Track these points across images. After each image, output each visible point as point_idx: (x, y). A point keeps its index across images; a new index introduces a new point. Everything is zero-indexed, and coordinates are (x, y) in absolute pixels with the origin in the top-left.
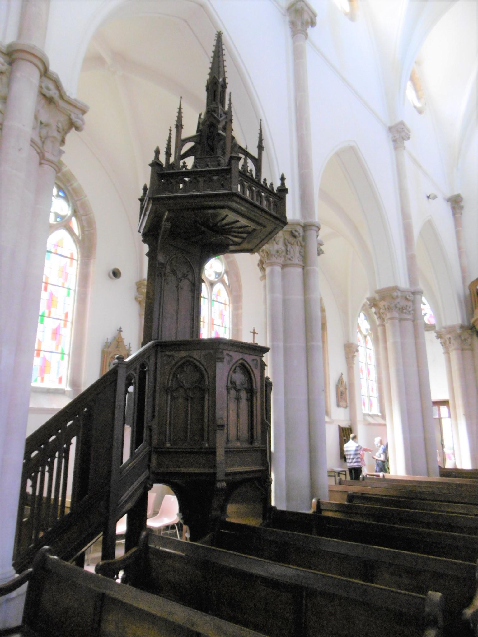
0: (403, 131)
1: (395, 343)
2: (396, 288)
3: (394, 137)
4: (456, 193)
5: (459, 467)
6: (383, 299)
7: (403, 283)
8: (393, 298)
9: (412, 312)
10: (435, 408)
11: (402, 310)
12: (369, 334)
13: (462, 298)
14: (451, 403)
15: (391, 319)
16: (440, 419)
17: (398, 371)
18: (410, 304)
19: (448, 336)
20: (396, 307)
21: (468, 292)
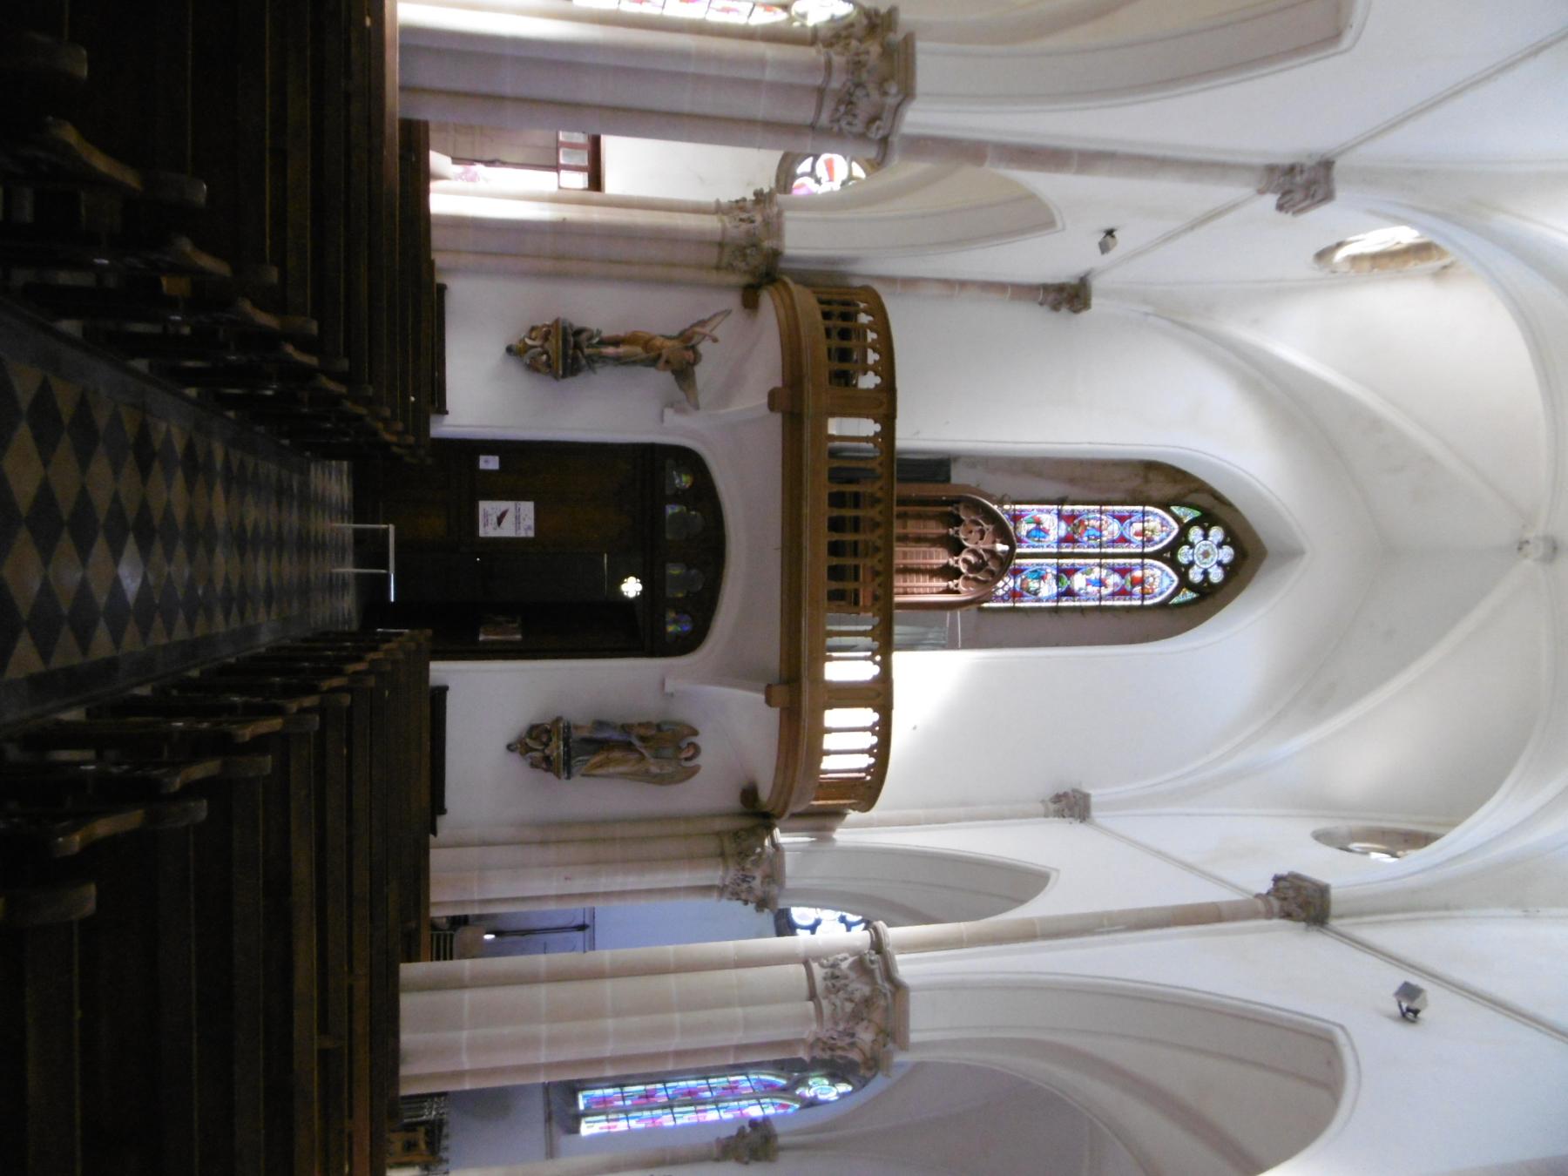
0: (1306, 197)
1: (762, 63)
2: (908, 94)
3: (1302, 172)
4: (1095, 301)
5: (434, 185)
6: (888, 52)
7: (918, 118)
8: (882, 83)
9: (836, 129)
10: (580, 138)
11: (847, 101)
12: (791, 19)
13: (842, 268)
14: (595, 195)
15: (829, 66)
16: (556, 168)
17: (685, 55)
18: (859, 126)
19: (758, 218)
20: (859, 85)
21: (857, 283)
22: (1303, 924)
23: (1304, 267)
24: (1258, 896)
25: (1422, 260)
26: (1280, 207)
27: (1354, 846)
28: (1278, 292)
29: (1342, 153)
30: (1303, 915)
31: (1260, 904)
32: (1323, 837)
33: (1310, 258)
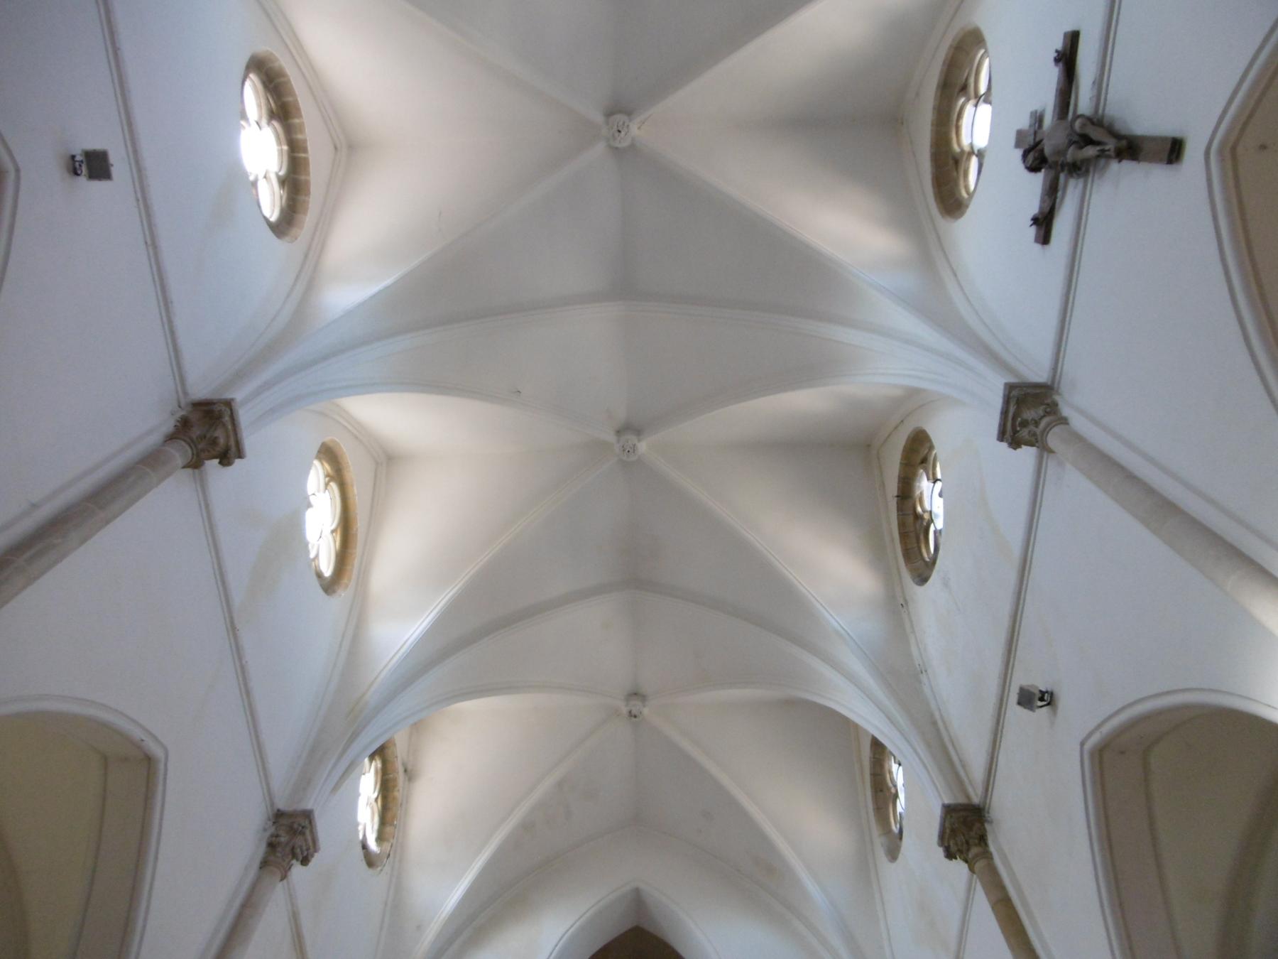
0: (302, 833)
22: (987, 826)
23: (378, 880)
24: (972, 870)
25: (395, 786)
26: (305, 861)
28: (396, 905)
29: (272, 804)
30: (977, 825)
31: (979, 865)
33: (371, 871)
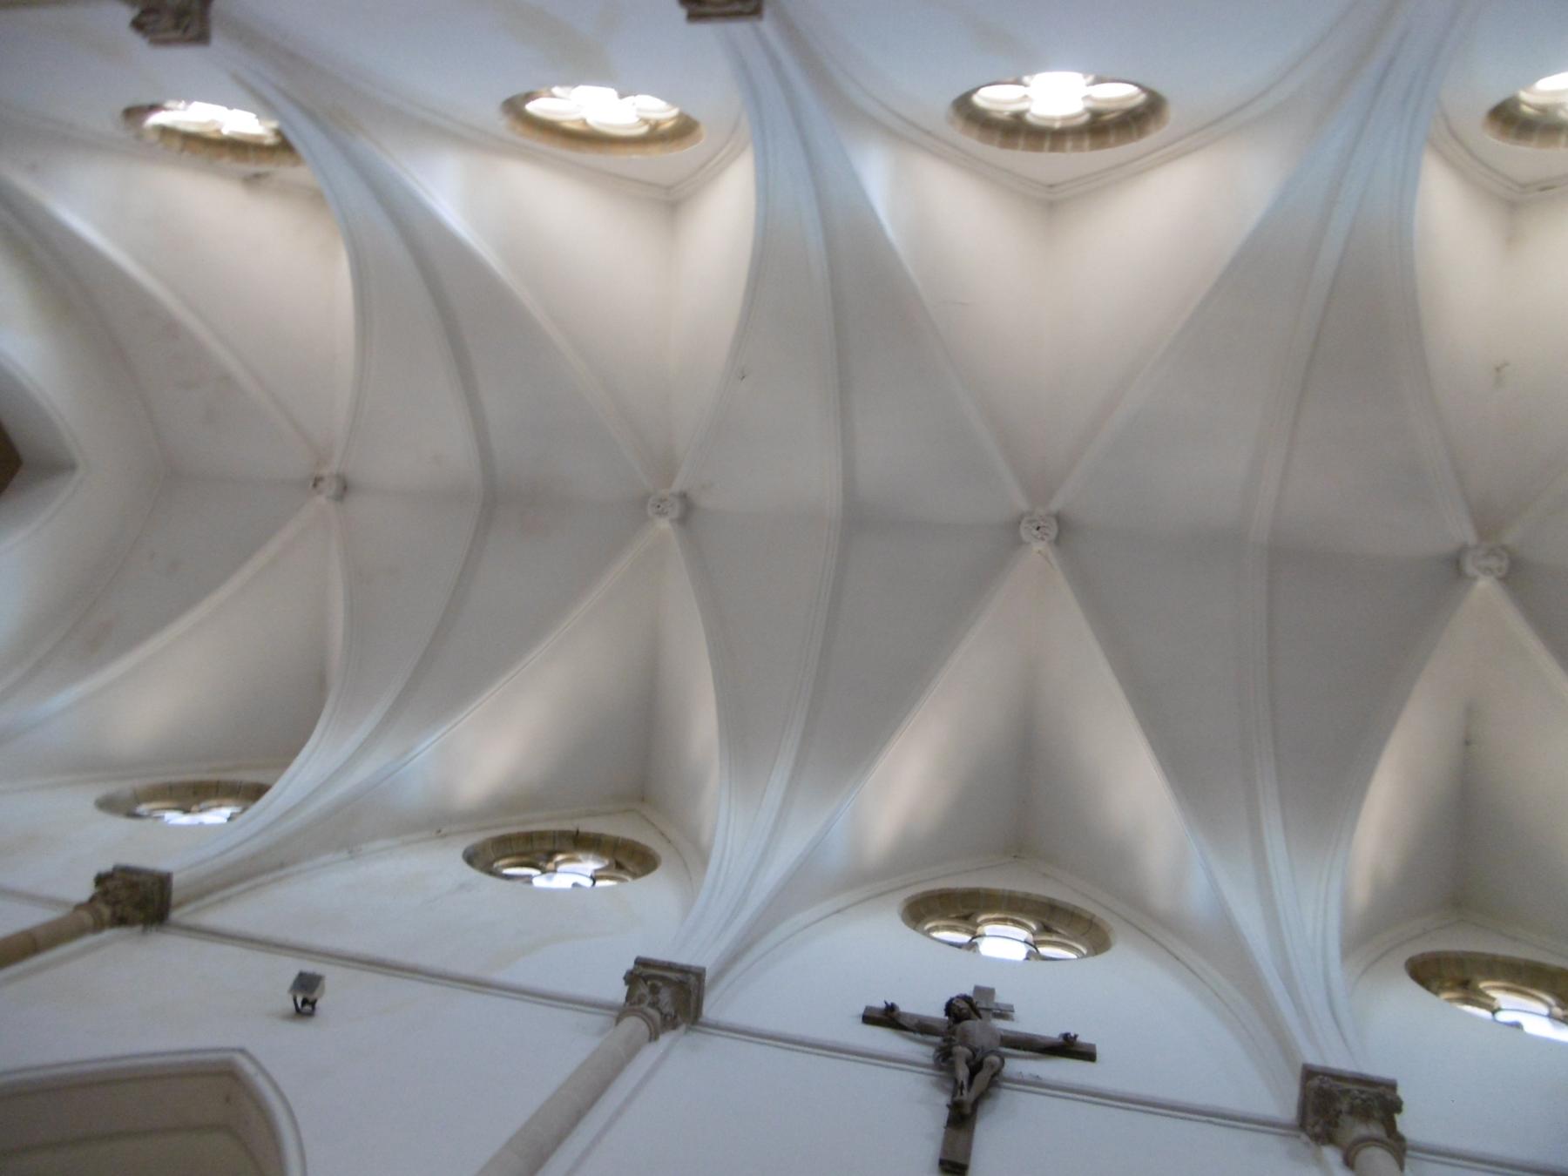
22: (139, 928)
24: (79, 907)
27: (143, 808)
32: (108, 805)
